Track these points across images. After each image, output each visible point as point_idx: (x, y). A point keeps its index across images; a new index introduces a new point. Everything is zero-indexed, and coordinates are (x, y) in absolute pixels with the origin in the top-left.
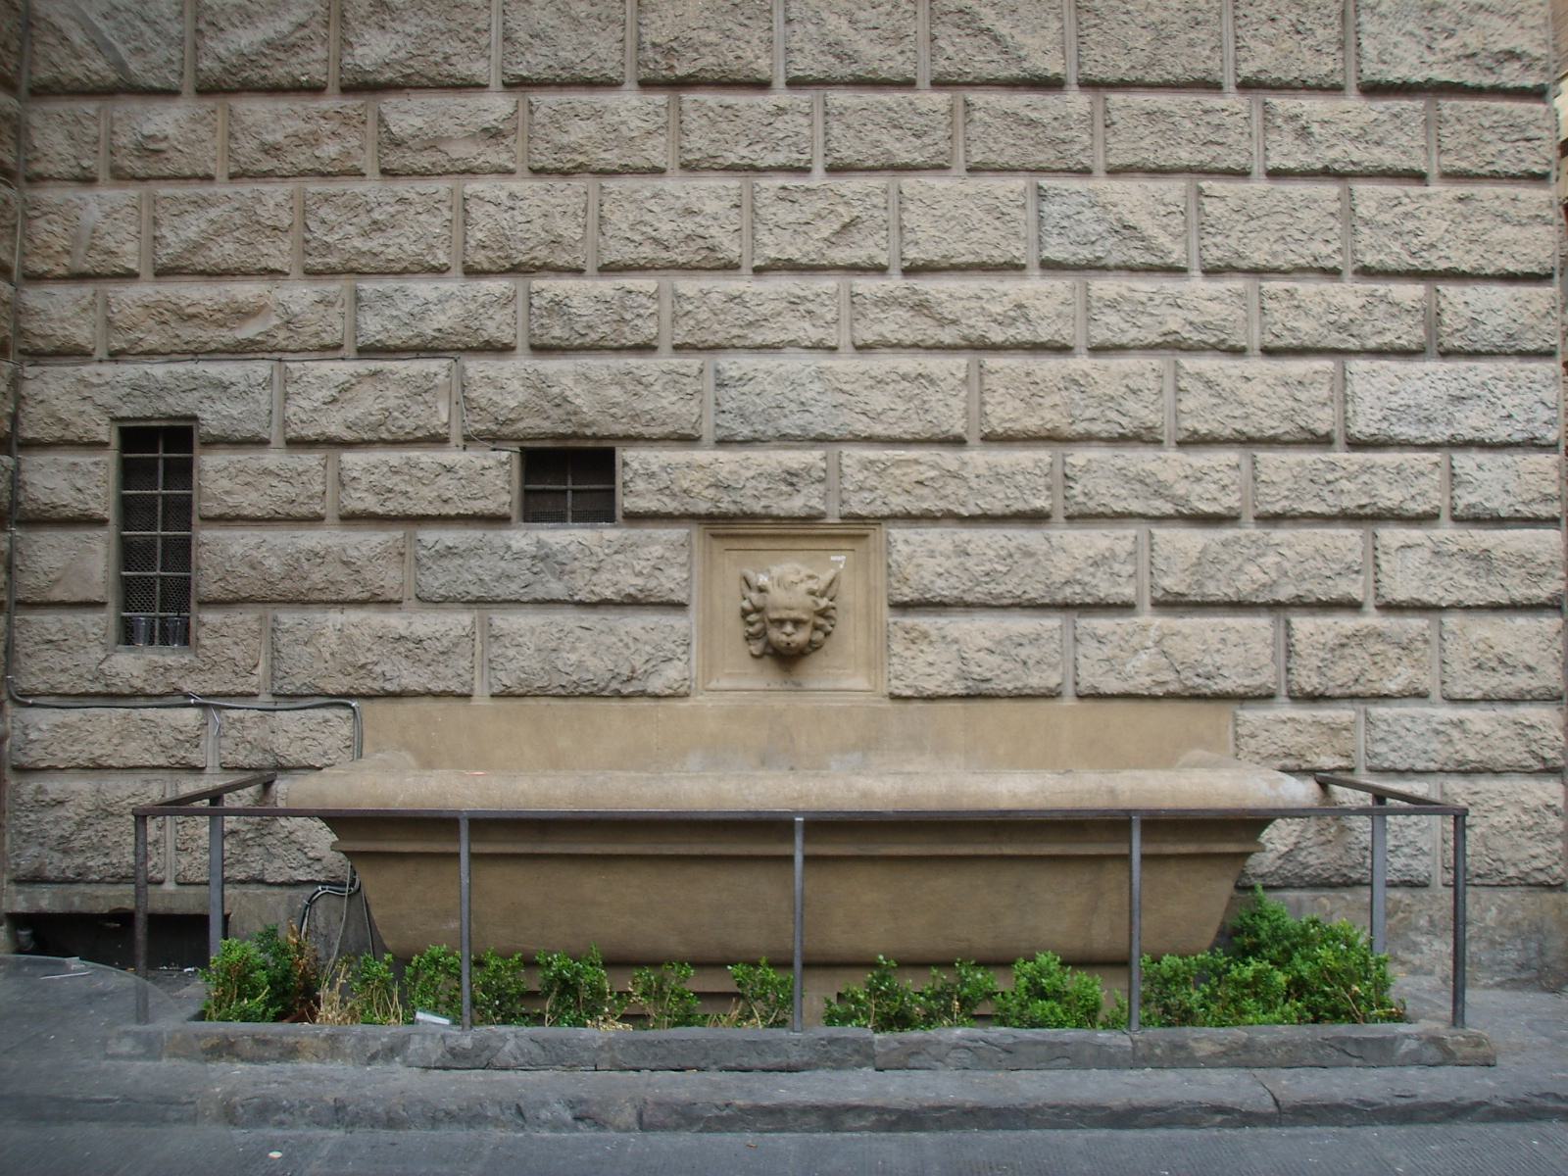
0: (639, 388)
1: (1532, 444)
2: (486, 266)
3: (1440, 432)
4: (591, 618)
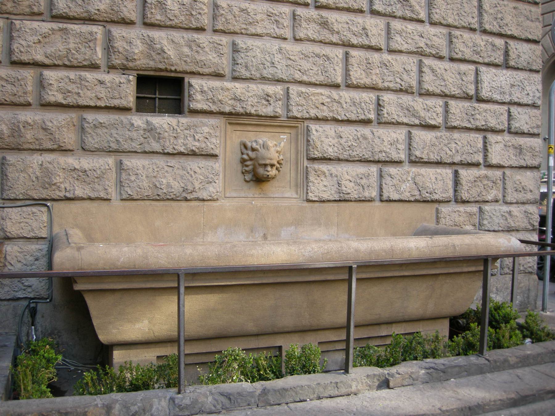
0: (199, 49)
3: (507, 99)
4: (173, 161)
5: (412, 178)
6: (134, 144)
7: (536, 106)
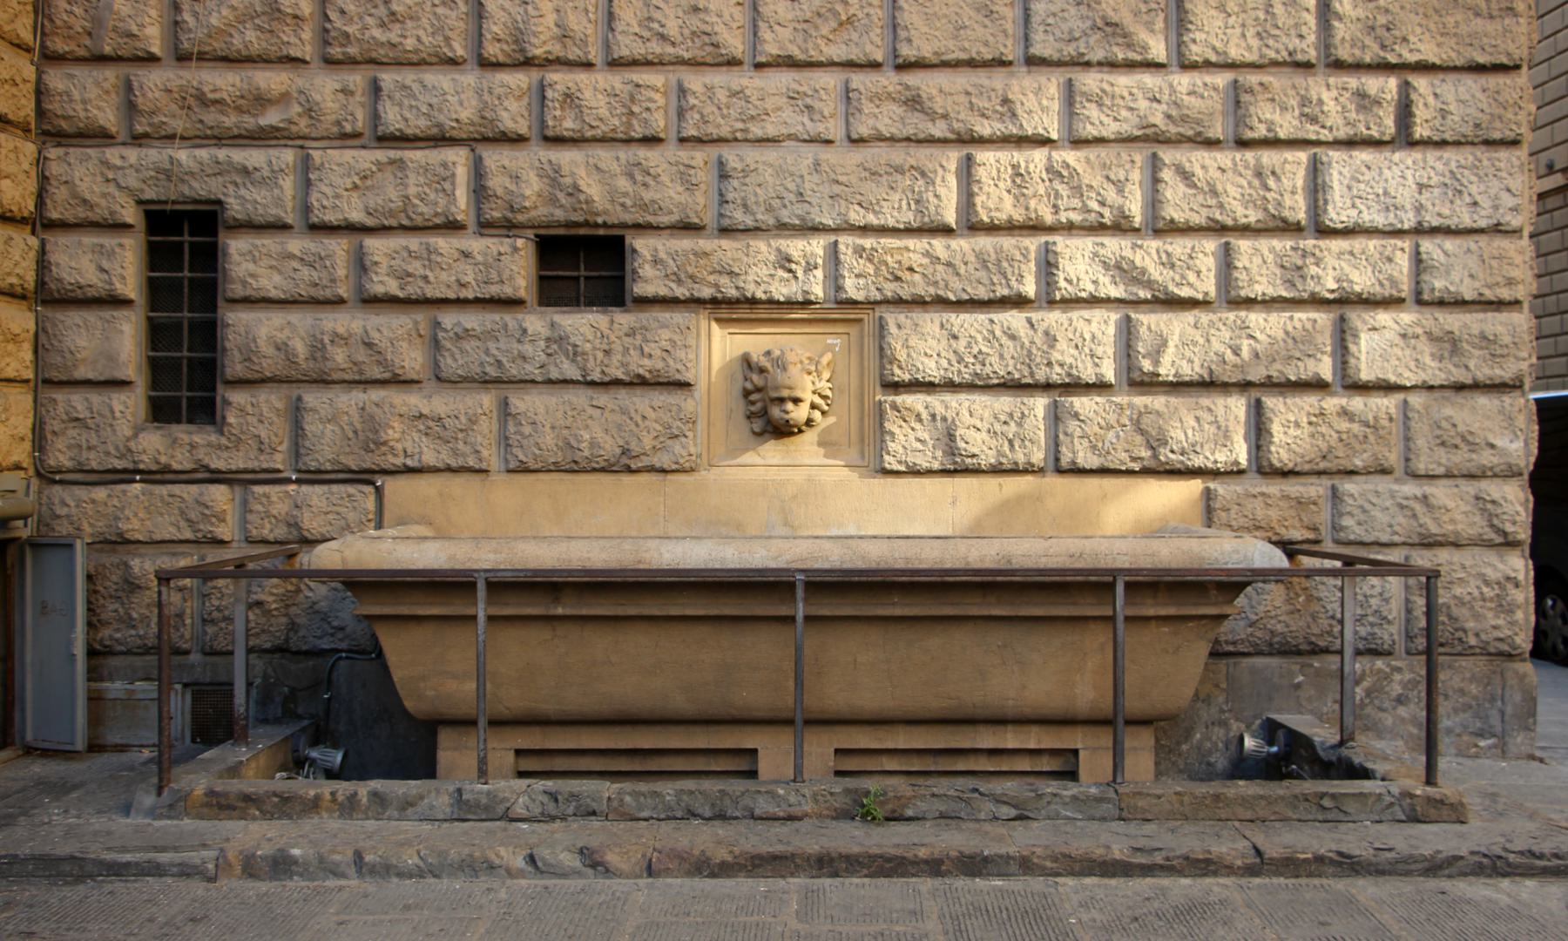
0: (648, 180)
1: (1497, 229)
2: (501, 59)
4: (603, 398)
5: (1131, 420)
6: (529, 368)
7: (1507, 232)
